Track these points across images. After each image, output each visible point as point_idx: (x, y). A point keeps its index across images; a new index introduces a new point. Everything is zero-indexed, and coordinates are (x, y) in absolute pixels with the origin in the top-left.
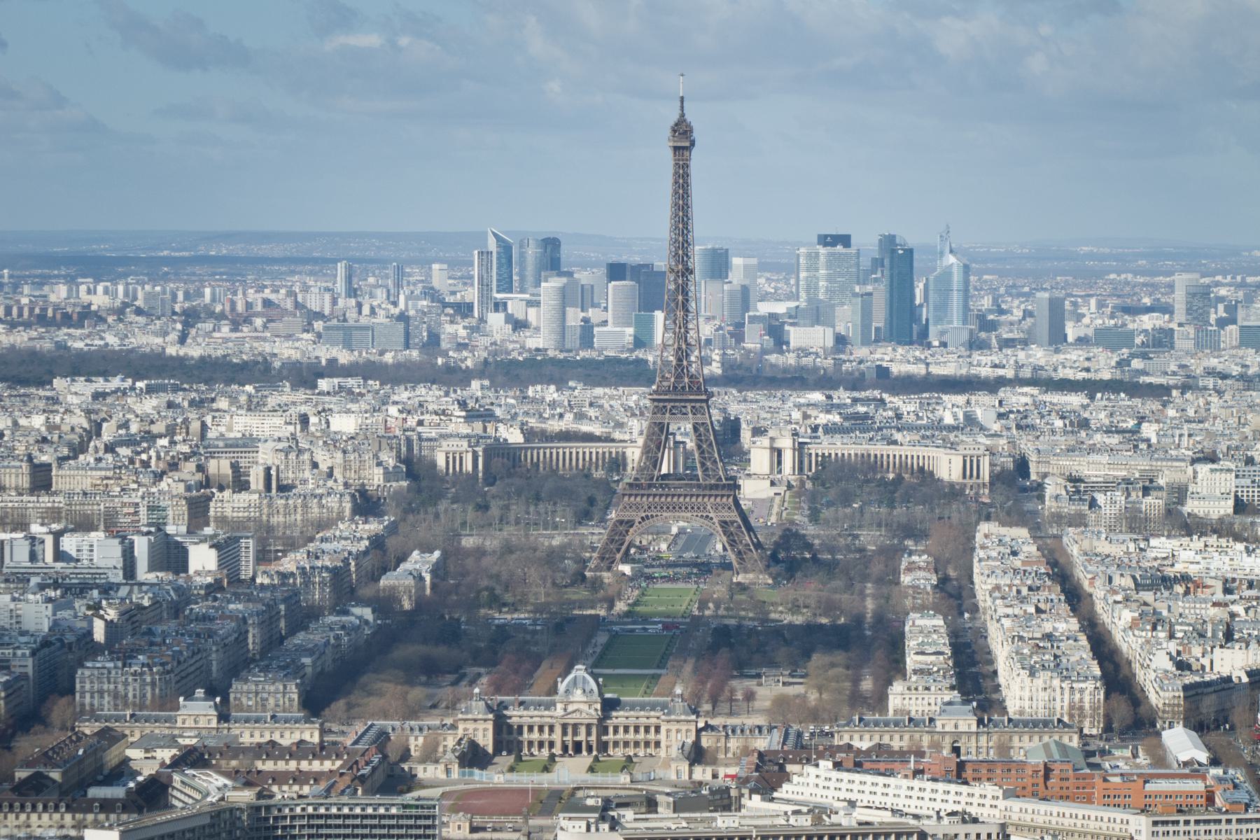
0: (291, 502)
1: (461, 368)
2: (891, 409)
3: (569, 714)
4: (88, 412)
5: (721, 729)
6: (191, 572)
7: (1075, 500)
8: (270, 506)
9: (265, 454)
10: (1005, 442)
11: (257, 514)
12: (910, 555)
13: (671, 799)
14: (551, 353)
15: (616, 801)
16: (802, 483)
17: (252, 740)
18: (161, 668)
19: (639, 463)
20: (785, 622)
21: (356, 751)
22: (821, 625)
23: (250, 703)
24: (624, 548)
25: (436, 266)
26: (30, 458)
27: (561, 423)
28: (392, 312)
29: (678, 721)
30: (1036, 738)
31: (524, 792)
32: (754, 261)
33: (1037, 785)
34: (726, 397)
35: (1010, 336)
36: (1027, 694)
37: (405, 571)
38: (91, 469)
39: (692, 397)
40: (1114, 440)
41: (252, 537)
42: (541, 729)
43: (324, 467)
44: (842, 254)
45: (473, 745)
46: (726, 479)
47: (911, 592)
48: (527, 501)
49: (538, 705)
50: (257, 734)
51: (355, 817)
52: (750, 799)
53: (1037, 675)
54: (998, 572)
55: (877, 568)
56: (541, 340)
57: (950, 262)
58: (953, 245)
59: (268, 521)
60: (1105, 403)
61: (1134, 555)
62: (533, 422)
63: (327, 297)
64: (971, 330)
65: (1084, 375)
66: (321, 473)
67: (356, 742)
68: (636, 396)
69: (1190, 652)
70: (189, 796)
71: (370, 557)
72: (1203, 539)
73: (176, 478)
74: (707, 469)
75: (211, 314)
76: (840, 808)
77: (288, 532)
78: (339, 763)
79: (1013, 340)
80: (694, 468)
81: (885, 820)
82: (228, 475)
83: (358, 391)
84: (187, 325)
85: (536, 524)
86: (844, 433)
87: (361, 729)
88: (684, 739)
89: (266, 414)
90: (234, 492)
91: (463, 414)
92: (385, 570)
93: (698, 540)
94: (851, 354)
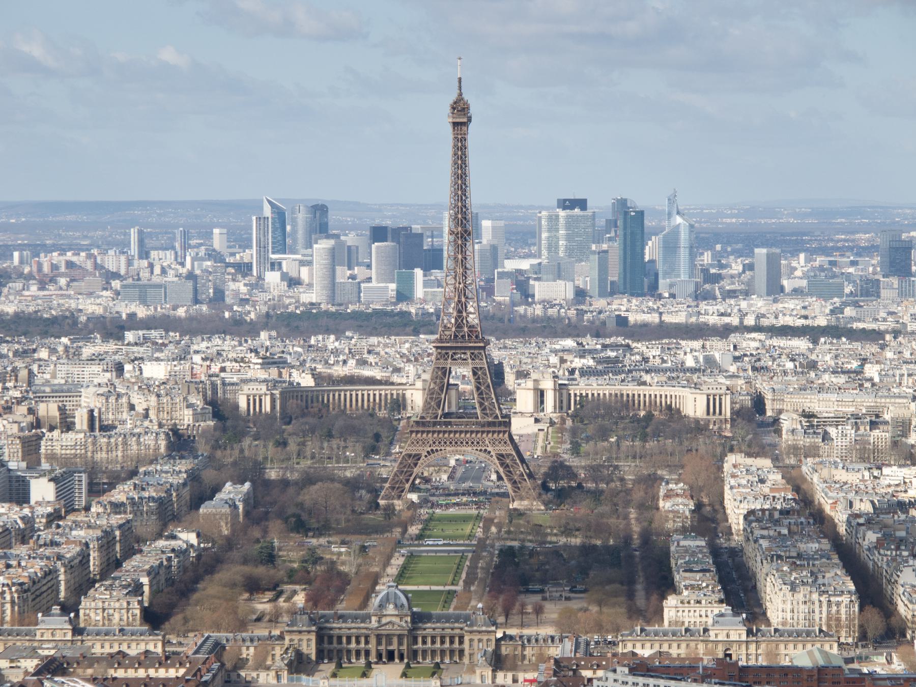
0: (112, 440)
1: (246, 321)
5: (518, 639)
6: (32, 502)
7: (809, 433)
8: (94, 444)
9: (88, 398)
10: (743, 382)
11: (83, 451)
12: (667, 483)
16: (563, 421)
17: (103, 651)
18: (19, 588)
20: (561, 543)
22: (595, 546)
23: (98, 618)
24: (412, 478)
25: (216, 231)
27: (345, 369)
28: (181, 271)
30: (800, 646)
35: (732, 287)
37: (222, 500)
40: (841, 380)
42: (349, 639)
43: (140, 409)
44: (580, 216)
45: (299, 654)
46: (502, 417)
47: (671, 516)
48: (321, 436)
50: (107, 645)
53: (798, 589)
55: (638, 495)
56: (314, 296)
57: (677, 223)
58: (679, 208)
59: (92, 457)
60: (828, 347)
61: (869, 482)
62: (320, 368)
63: (123, 259)
64: (697, 283)
66: (138, 414)
67: (196, 652)
71: (188, 488)
73: (11, 420)
75: (21, 275)
77: (110, 467)
78: (182, 671)
79: (734, 291)
83: (160, 341)
85: (329, 458)
86: (598, 375)
88: (485, 647)
90: (62, 432)
91: (260, 361)
93: (473, 472)
94: (591, 305)
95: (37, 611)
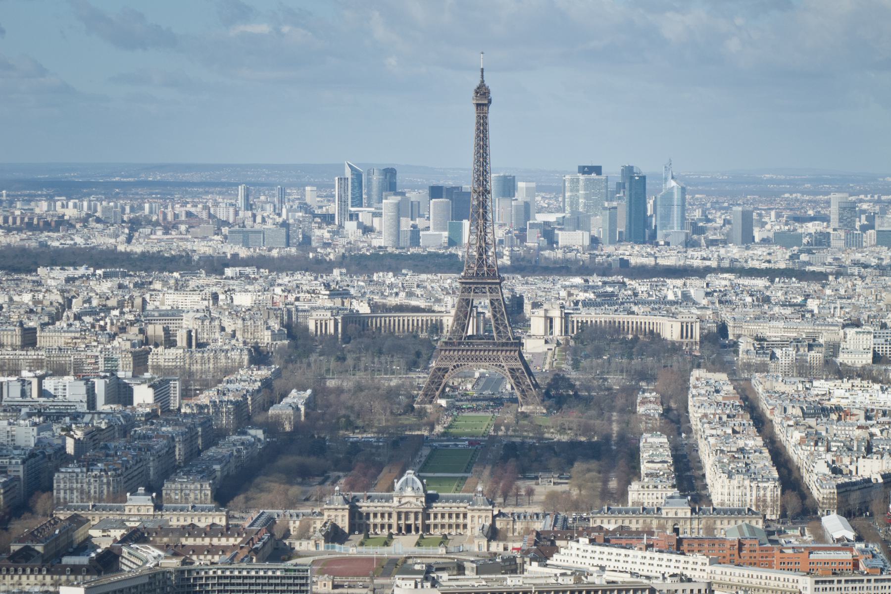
0: (205, 355)
1: (326, 260)
2: (630, 289)
3: (403, 505)
4: (62, 291)
5: (510, 515)
6: (135, 404)
7: (760, 353)
8: (191, 358)
9: (188, 321)
10: (711, 312)
11: (182, 363)
12: (644, 392)
13: (475, 565)
14: (390, 250)
15: (435, 566)
16: (567, 342)
17: (178, 523)
18: (114, 472)
19: (452, 327)
20: (555, 440)
21: (252, 531)
22: (581, 442)
23: (177, 497)
24: (441, 387)
25: (308, 188)
26: (21, 324)
27: (396, 299)
28: (277, 221)
29: (479, 510)
30: (733, 522)
31: (370, 560)
32: (533, 185)
33: (734, 555)
34: (514, 281)
35: (715, 237)
36: (726, 491)
37: (287, 404)
38: (65, 332)
39: (489, 281)
40: (788, 311)
41: (178, 380)
42: (383, 515)
43: (229, 330)
44: (595, 180)
45: (335, 527)
46: (514, 339)
47: (644, 418)
49: (381, 499)
50: (182, 519)
51: (251, 578)
52: (531, 565)
53: (733, 477)
54: (706, 404)
55: (620, 402)
56: (382, 240)
57: (672, 186)
58: (674, 174)
59: (190, 368)
60: (781, 285)
61: (802, 392)
62: (377, 299)
63: (231, 210)
64: (687, 234)
65: (767, 265)
66: (227, 334)
67: (252, 525)
68: (450, 280)
69: (841, 461)
70: (134, 563)
72: (851, 381)
73: (125, 338)
74: (500, 332)
75: (149, 222)
76: (594, 572)
78: (239, 540)
79: (716, 240)
80: (490, 331)
81: (626, 580)
82: (161, 336)
83: (253, 276)
84: (132, 230)
85: (379, 371)
86: (597, 306)
87: (255, 516)
88: (484, 522)
89: (188, 293)
90: (165, 348)
91: (328, 292)
92: (272, 403)
93: (494, 382)
94: (602, 250)
95: (128, 491)
